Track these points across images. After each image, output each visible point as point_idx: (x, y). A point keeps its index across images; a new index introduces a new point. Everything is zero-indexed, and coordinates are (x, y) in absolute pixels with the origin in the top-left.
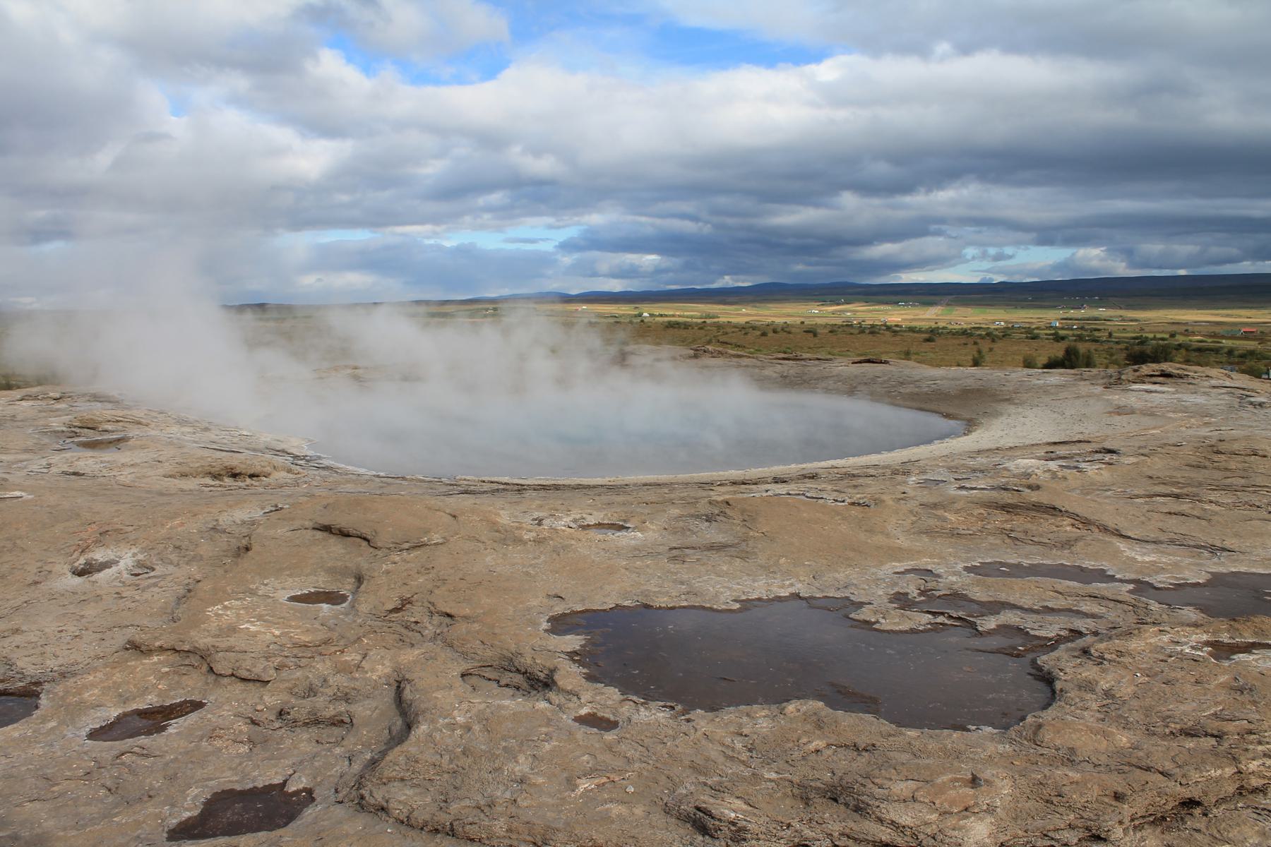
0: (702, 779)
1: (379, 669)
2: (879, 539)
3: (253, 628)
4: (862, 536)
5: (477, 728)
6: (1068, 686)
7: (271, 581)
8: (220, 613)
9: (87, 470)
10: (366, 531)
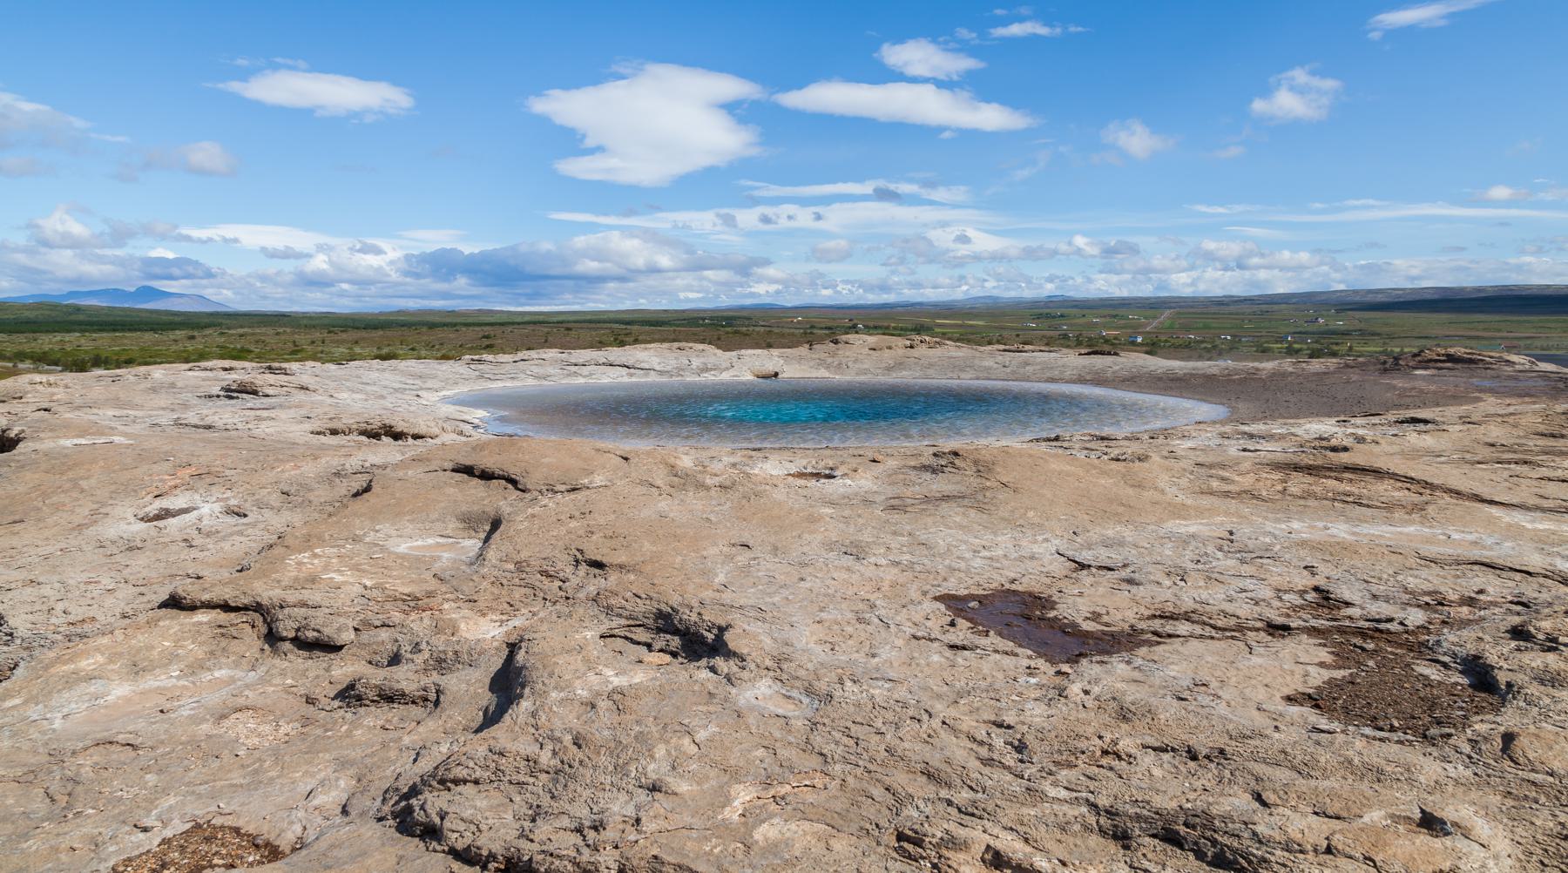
0: (944, 793)
1: (486, 631)
2: (1148, 495)
3: (338, 578)
4: (1130, 491)
5: (603, 704)
6: (1519, 678)
7: (386, 528)
8: (299, 563)
9: (220, 424)
10: (513, 471)
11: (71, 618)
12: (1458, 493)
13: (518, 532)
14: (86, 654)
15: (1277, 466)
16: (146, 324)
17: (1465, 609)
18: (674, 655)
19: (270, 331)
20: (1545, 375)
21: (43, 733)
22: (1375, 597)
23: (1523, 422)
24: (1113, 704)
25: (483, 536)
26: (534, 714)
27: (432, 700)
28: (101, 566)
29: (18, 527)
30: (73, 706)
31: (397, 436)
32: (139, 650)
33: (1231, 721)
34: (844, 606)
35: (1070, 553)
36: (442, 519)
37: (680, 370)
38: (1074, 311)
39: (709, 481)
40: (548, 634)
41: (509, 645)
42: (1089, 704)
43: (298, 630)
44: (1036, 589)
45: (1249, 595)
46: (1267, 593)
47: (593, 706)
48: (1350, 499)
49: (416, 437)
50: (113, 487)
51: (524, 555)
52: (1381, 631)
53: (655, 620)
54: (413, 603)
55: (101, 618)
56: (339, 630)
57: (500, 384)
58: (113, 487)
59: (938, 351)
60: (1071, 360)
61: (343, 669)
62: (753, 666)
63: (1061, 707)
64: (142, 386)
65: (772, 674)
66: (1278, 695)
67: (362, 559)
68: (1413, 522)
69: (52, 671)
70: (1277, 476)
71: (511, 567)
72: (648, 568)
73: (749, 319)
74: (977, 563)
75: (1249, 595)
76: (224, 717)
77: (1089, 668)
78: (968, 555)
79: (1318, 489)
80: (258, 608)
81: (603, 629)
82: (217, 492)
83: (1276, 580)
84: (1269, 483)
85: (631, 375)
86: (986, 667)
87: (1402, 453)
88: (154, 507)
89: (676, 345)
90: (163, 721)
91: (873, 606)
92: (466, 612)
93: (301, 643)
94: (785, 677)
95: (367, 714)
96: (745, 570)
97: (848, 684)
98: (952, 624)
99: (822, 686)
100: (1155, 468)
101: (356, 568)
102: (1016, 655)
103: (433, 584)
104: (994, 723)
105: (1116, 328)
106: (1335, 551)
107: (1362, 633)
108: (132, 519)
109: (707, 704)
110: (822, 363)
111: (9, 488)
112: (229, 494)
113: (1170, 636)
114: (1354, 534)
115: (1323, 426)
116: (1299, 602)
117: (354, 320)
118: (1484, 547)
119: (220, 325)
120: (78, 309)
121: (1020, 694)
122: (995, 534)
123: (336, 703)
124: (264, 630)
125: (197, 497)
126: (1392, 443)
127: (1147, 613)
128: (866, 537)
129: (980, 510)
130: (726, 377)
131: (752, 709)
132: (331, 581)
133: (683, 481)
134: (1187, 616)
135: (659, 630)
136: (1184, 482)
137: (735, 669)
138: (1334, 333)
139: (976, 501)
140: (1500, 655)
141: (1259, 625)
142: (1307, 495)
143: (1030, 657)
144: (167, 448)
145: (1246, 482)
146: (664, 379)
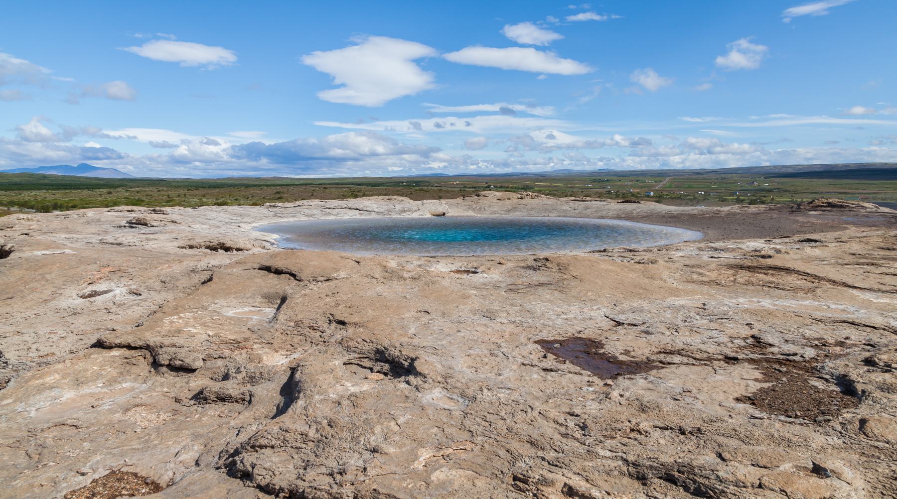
0: (540, 453)
1: (278, 361)
2: (657, 283)
3: (193, 330)
4: (647, 281)
5: (345, 403)
6: (869, 388)
7: (221, 302)
8: (171, 322)
9: (126, 242)
10: (294, 269)
11: (41, 353)
12: (834, 282)
13: (297, 304)
14: (49, 374)
15: (730, 266)
16: (84, 185)
17: (838, 348)
18: (386, 374)
19: (155, 189)
20: (884, 215)
21: (25, 419)
22: (786, 341)
23: (871, 241)
24: (637, 402)
25: (276, 306)
26: (305, 408)
27: (247, 400)
28: (58, 323)
29: (10, 301)
30: (42, 403)
31: (227, 249)
32: (79, 372)
33: (704, 412)
34: (483, 346)
35: (612, 316)
36: (253, 297)
37: (389, 212)
38: (614, 178)
39: (405, 275)
40: (314, 362)
41: (291, 369)
42: (623, 402)
43: (170, 360)
44: (593, 336)
45: (715, 340)
46: (725, 339)
47: (339, 404)
48: (772, 285)
49: (238, 250)
50: (65, 279)
51: (300, 317)
52: (790, 361)
53: (375, 355)
54: (236, 345)
55: (58, 353)
56: (194, 360)
57: (286, 220)
58: (65, 279)
59: (537, 201)
60: (613, 206)
61: (196, 383)
62: (431, 381)
63: (607, 404)
64: (81, 221)
65: (441, 385)
66: (731, 397)
67: (207, 319)
68: (808, 299)
69: (30, 383)
70: (731, 272)
71: (292, 324)
72: (371, 325)
73: (428, 182)
74: (559, 322)
75: (715, 340)
76: (128, 410)
77: (623, 382)
78: (554, 317)
79: (754, 280)
80: (147, 347)
81: (345, 359)
82: (124, 281)
83: (730, 332)
84: (726, 276)
85: (361, 214)
86: (564, 381)
87: (802, 259)
88: (88, 290)
89: (387, 197)
90: (93, 412)
91: (499, 347)
92: (266, 350)
93: (172, 368)
94: (449, 387)
95: (210, 408)
96: (426, 326)
97: (485, 391)
98: (545, 357)
99: (470, 392)
100: (661, 268)
101: (204, 325)
102: (581, 374)
103: (248, 334)
104: (569, 413)
105: (638, 188)
106: (764, 315)
107: (779, 362)
108: (76, 297)
109: (404, 402)
110: (470, 208)
111: (5, 279)
112: (131, 282)
113: (669, 363)
114: (774, 305)
115: (757, 244)
116: (743, 344)
117: (202, 183)
118: (849, 313)
119: (126, 186)
120: (45, 177)
121: (583, 397)
122: (569, 305)
123: (192, 402)
124: (151, 360)
125: (113, 284)
126: (797, 253)
127: (656, 350)
128: (496, 307)
129: (561, 291)
130: (415, 215)
131: (430, 405)
132: (189, 332)
133: (391, 275)
134: (679, 352)
135: (377, 360)
136: (677, 275)
137: (421, 382)
138: (763, 190)
139: (558, 286)
140: (858, 374)
141: (720, 357)
142: (748, 283)
143: (589, 376)
144: (96, 256)
145: (713, 275)
146: (380, 217)
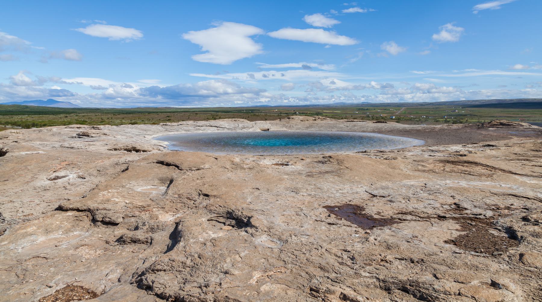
0: (326, 274)
1: (168, 218)
2: (397, 171)
3: (117, 200)
4: (391, 170)
5: (208, 244)
6: (525, 235)
7: (133, 183)
8: (103, 195)
9: (76, 147)
10: (177, 163)
11: (25, 214)
12: (504, 171)
13: (179, 184)
14: (30, 226)
15: (441, 161)
16: (51, 112)
17: (506, 211)
18: (233, 226)
19: (93, 114)
20: (534, 130)
21: (15, 254)
22: (475, 206)
23: (526, 146)
24: (385, 244)
25: (167, 185)
26: (184, 247)
27: (149, 242)
28: (35, 196)
29: (6, 182)
30: (25, 244)
31: (137, 151)
32: (48, 225)
33: (426, 249)
34: (292, 210)
35: (370, 191)
36: (153, 180)
37: (235, 128)
38: (371, 108)
39: (245, 166)
40: (190, 219)
41: (176, 223)
42: (376, 244)
43: (103, 218)
44: (358, 204)
45: (432, 206)
46: (438, 205)
47: (205, 244)
48: (467, 173)
49: (144, 151)
50: (39, 169)
51: (181, 192)
52: (477, 218)
53: (227, 215)
54: (143, 209)
55: (35, 214)
56: (117, 218)
57: (173, 133)
58: (39, 169)
59: (324, 122)
60: (370, 125)
61: (119, 232)
62: (260, 230)
63: (367, 245)
64: (49, 134)
65: (267, 233)
66: (442, 241)
67: (125, 193)
68: (488, 181)
69: (18, 232)
70: (442, 165)
71: (177, 196)
72: (224, 197)
73: (259, 110)
74: (338, 195)
75: (432, 206)
76: (77, 248)
77: (376, 231)
78: (334, 192)
79: (455, 169)
80: (89, 210)
81: (209, 218)
82: (75, 170)
83: (441, 201)
84: (439, 167)
85: (218, 130)
86: (341, 231)
87: (485, 157)
88: (53, 175)
89: (234, 119)
90: (56, 249)
91: (302, 210)
92: (161, 212)
93: (104, 223)
94: (271, 234)
95: (127, 247)
96: (258, 197)
97: (293, 236)
98: (329, 216)
99: (284, 237)
100: (399, 162)
101: (123, 196)
102: (351, 227)
103: (150, 202)
104: (344, 250)
105: (386, 114)
106: (461, 190)
107: (471, 219)
108: (46, 180)
109: (244, 243)
110: (284, 126)
111: (3, 169)
112: (79, 171)
113: (404, 220)
114: (468, 185)
115: (457, 148)
116: (449, 208)
117: (122, 111)
118: (513, 189)
119: (76, 112)
120: (27, 107)
121: (352, 240)
122: (344, 185)
123: (116, 243)
124: (91, 218)
125: (68, 172)
126: (481, 153)
127: (397, 212)
128: (299, 186)
129: (339, 176)
130: (251, 130)
131: (260, 245)
132: (114, 201)
133: (236, 166)
134: (410, 213)
135: (228, 218)
136: (409, 167)
137: (254, 231)
138: (461, 115)
139: (337, 173)
140: (518, 227)
141: (435, 216)
142: (452, 171)
143: (356, 227)
144: (58, 155)
145: (431, 167)
146: (230, 131)
